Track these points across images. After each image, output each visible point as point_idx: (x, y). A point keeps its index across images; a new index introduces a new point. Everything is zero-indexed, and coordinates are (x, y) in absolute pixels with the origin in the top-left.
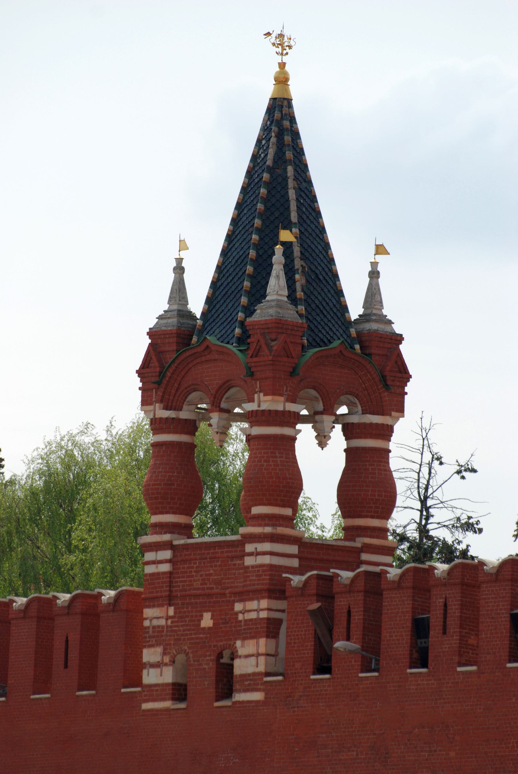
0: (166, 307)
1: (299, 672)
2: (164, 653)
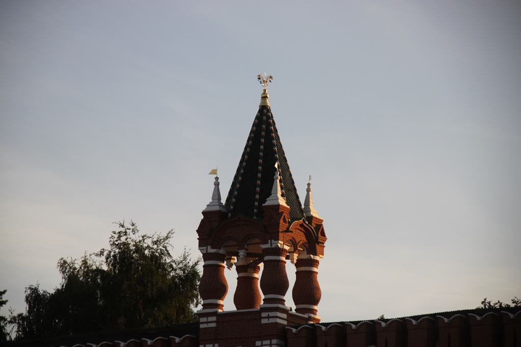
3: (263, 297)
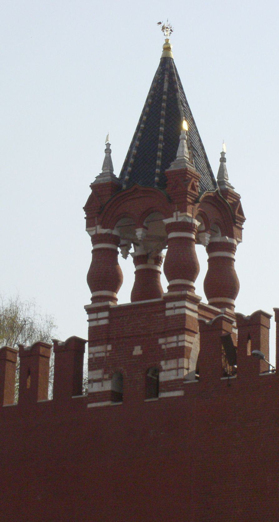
0: (101, 172)
2: (105, 373)
3: (167, 284)
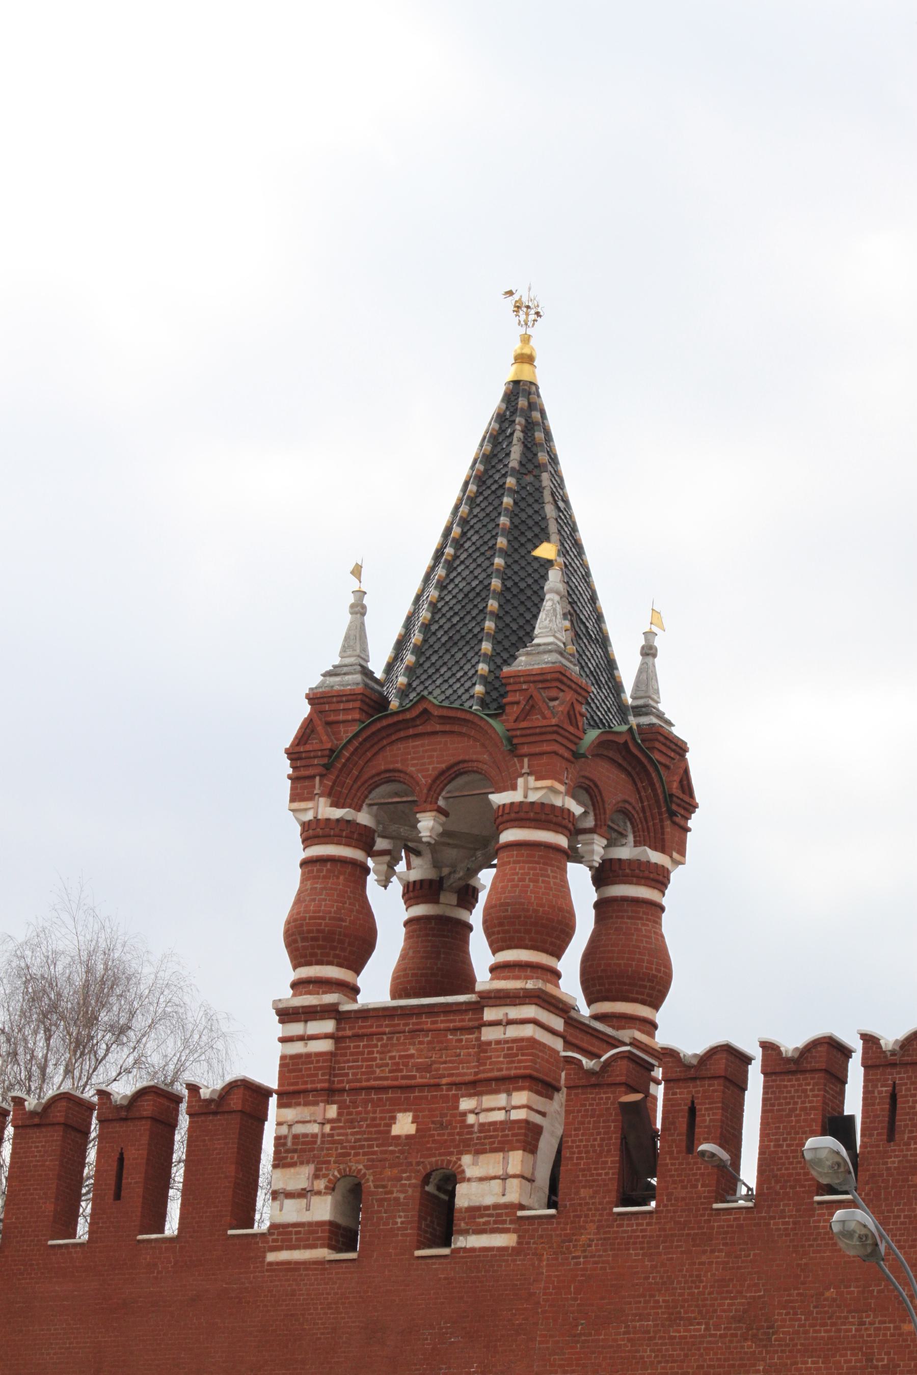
1: (587, 1204)
2: (316, 1176)
